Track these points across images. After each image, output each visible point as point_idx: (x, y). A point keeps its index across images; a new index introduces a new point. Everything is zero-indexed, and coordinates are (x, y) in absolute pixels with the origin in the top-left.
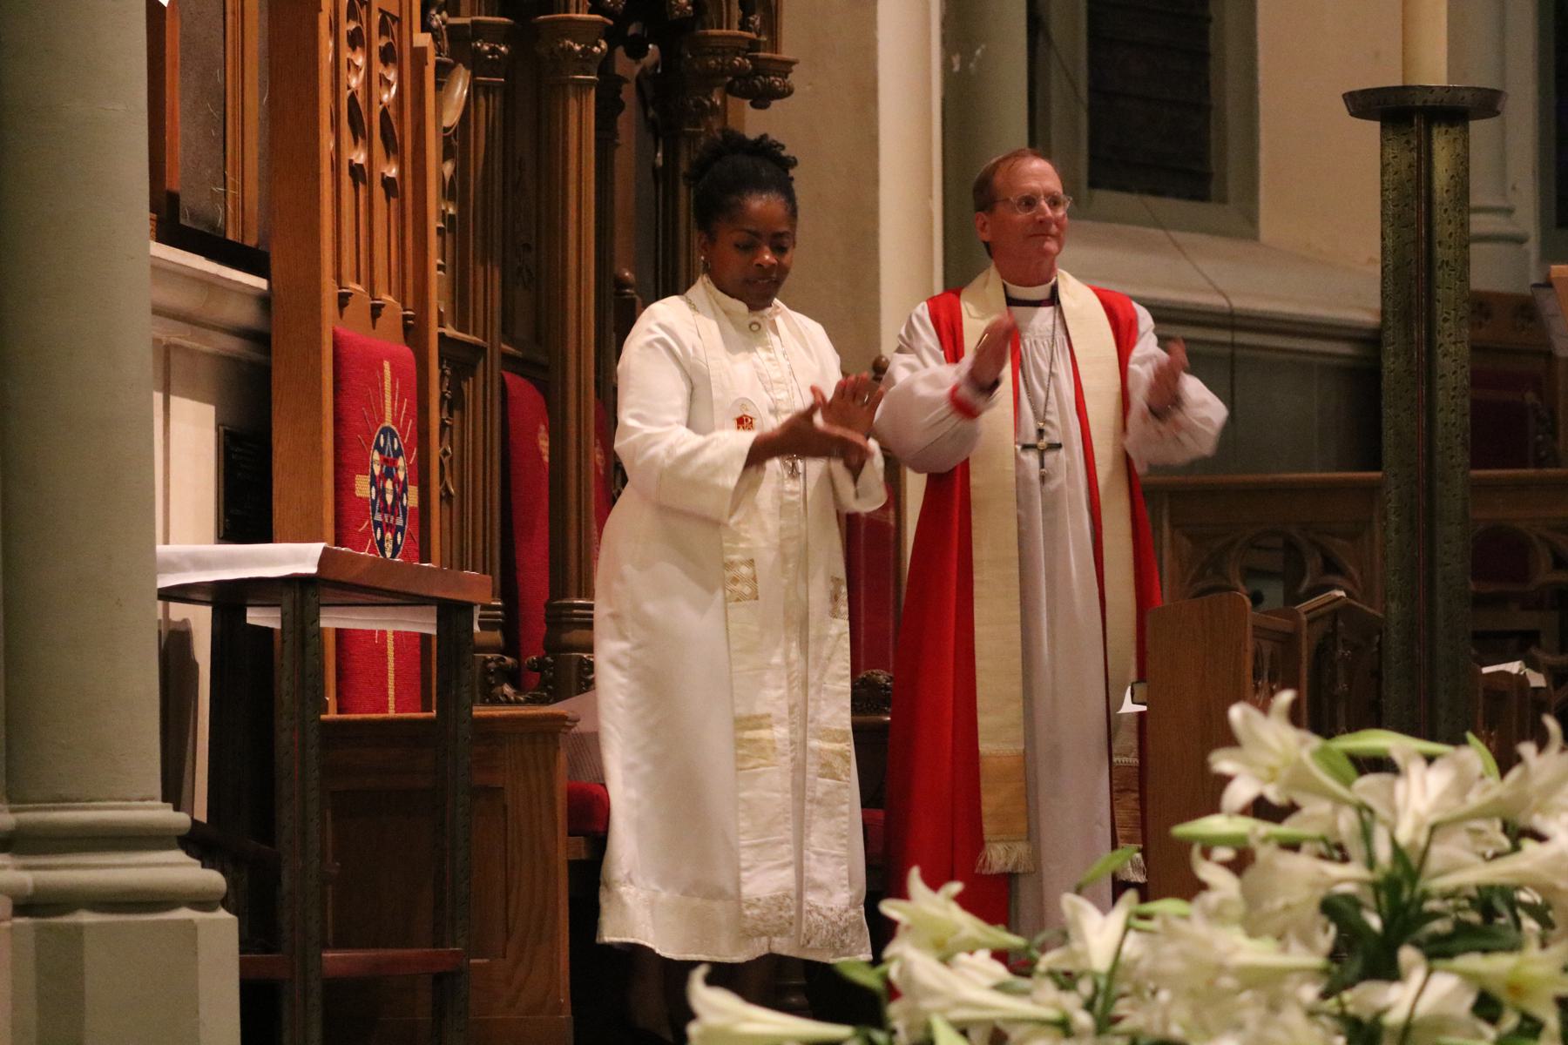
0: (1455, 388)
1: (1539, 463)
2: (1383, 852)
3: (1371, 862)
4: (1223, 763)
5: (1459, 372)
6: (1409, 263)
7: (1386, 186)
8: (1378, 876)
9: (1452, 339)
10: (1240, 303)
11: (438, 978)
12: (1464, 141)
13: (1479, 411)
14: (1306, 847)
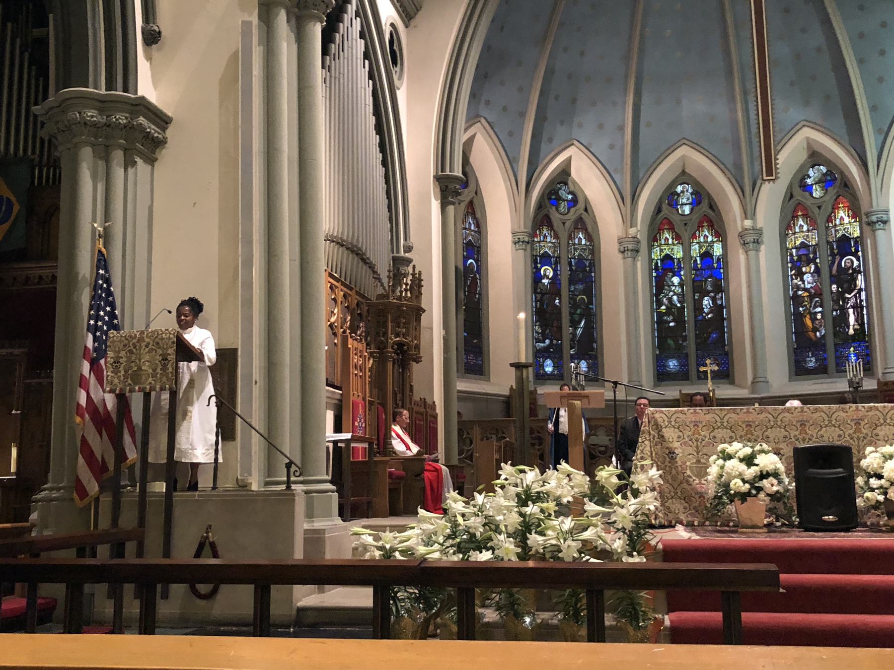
2: (525, 486)
3: (523, 488)
4: (500, 472)
10: (488, 392)
11: (368, 502)
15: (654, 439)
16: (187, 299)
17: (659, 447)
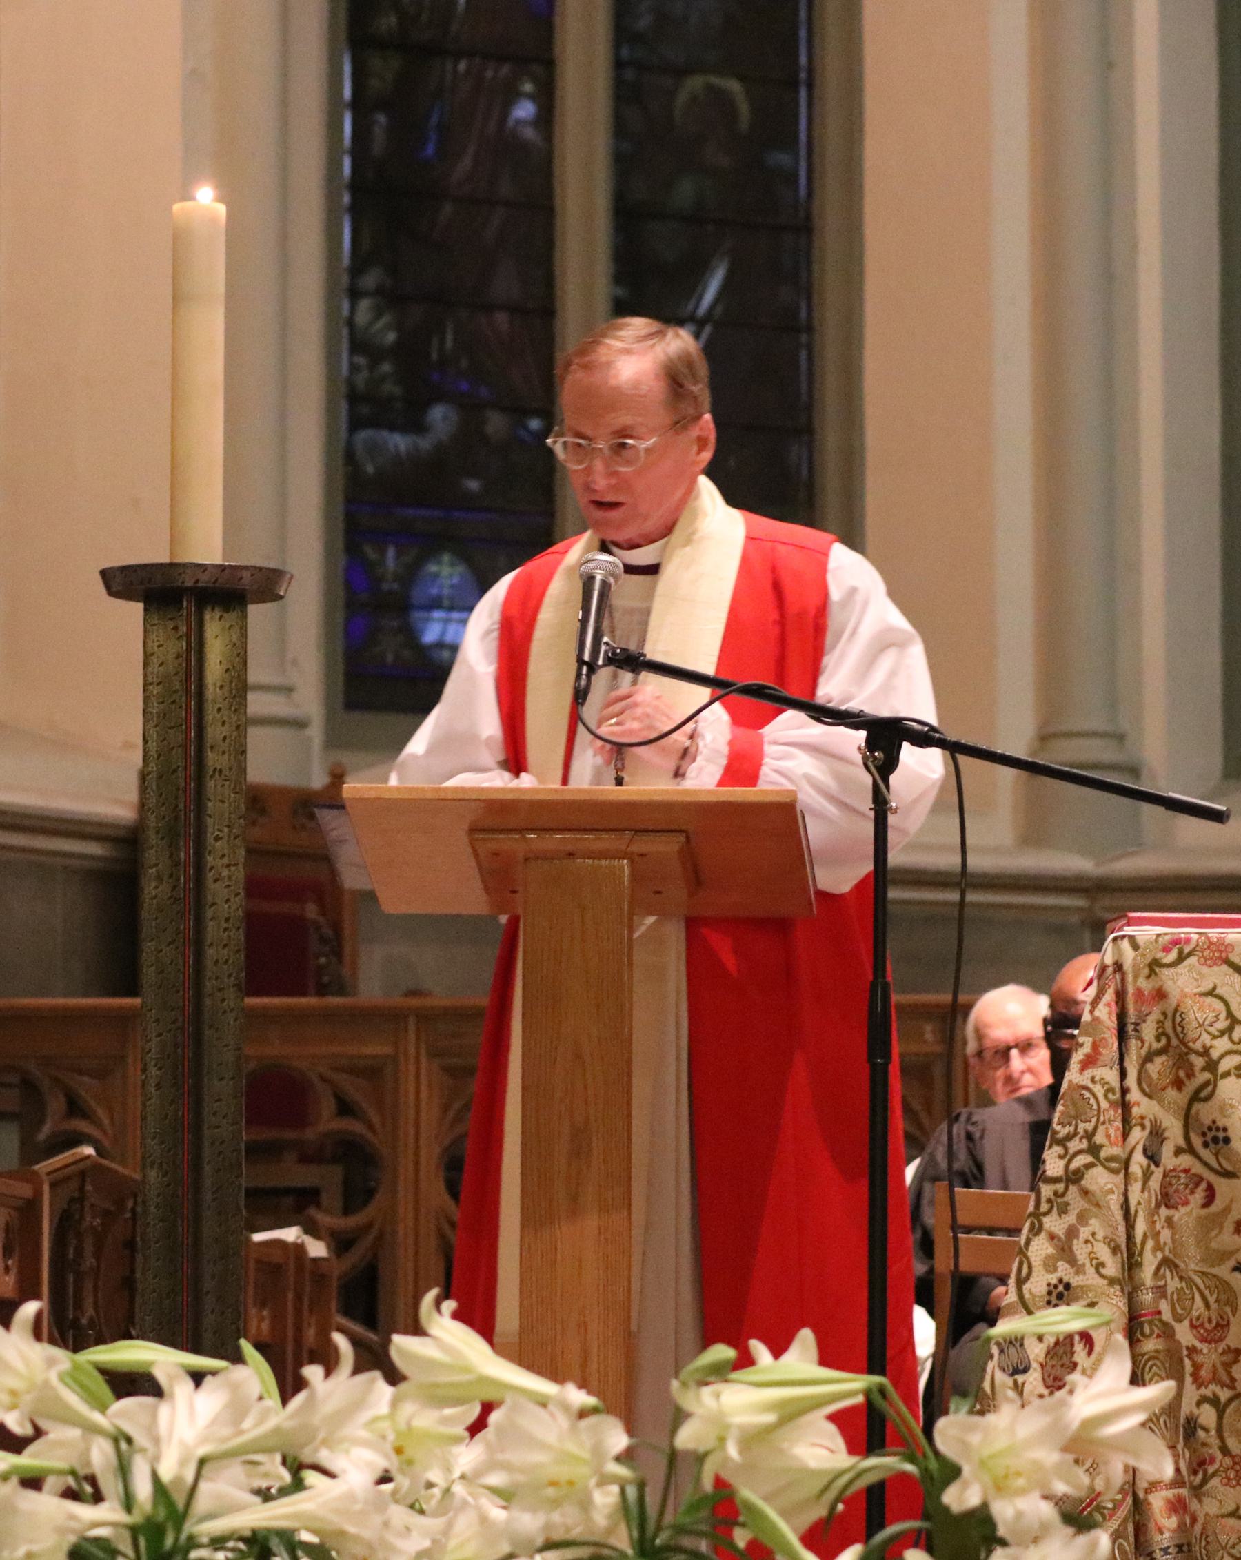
0: (227, 920)
1: (322, 991)
2: (143, 1490)
3: (128, 1503)
5: (232, 900)
6: (174, 771)
7: (150, 680)
8: (136, 1518)
9: (225, 861)
12: (241, 628)
13: (255, 924)
14: (50, 1483)
15: (1153, 1157)
16: (576, 664)
17: (1188, 1213)
